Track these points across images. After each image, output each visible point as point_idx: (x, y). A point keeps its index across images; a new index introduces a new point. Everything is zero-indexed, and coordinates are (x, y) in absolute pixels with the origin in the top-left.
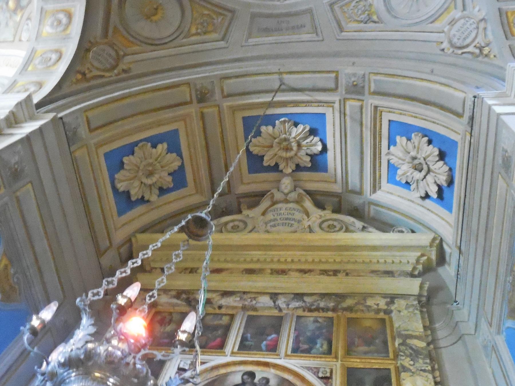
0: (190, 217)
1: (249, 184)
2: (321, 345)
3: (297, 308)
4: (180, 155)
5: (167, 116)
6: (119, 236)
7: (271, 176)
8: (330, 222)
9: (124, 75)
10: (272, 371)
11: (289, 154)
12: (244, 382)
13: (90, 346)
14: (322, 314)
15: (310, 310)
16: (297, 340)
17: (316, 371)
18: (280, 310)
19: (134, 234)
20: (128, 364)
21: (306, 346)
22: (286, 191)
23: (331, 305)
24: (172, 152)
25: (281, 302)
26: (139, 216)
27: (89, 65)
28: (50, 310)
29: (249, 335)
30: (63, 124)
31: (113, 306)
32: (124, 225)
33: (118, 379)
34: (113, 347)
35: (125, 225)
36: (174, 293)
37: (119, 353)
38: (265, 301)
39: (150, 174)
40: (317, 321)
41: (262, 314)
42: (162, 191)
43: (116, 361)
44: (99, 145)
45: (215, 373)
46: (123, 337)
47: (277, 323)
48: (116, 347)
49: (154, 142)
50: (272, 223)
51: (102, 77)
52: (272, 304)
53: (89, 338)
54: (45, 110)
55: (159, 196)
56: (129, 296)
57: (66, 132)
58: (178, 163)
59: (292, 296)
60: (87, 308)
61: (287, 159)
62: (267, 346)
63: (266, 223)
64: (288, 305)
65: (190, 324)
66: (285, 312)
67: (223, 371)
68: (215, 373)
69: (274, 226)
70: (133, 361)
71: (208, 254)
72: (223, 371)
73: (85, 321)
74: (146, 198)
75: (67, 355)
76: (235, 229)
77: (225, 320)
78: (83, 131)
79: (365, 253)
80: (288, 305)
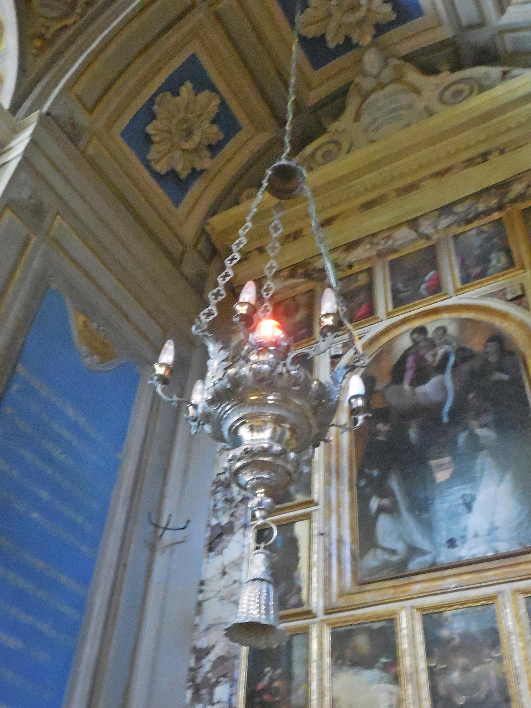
0: (269, 172)
1: (320, 84)
2: (497, 260)
3: (449, 226)
4: (213, 89)
5: (172, 41)
6: (189, 231)
7: (346, 59)
8: (454, 88)
9: (91, 11)
10: (446, 315)
11: (359, 15)
12: (416, 343)
13: (231, 371)
14: (484, 220)
15: (468, 222)
16: (464, 267)
17: (500, 294)
18: (428, 237)
19: (205, 222)
20: (281, 374)
21: (478, 270)
22: (375, 72)
23: (494, 202)
24: (201, 91)
25: (426, 227)
26: (201, 195)
27: (41, 21)
28: (168, 352)
29: (400, 285)
30: (54, 118)
31: (236, 319)
32: (188, 215)
33: (277, 394)
34: (256, 363)
35: (188, 216)
36: (286, 273)
37: (266, 367)
38: (404, 234)
39: (189, 134)
40: (482, 232)
41: (407, 252)
42: (214, 149)
43: (267, 376)
44: (109, 127)
45: (377, 346)
46: (262, 348)
47: (430, 257)
48: (261, 362)
49: (172, 86)
50: (373, 127)
51: (65, 27)
52: (412, 235)
53: (226, 364)
54: (24, 113)
55: (212, 157)
56: (246, 300)
57: (59, 128)
58: (216, 102)
59: (437, 213)
60: (207, 333)
61: (359, 24)
62: (427, 289)
63: (366, 131)
64: (435, 227)
65: (329, 304)
66: (435, 237)
67: (385, 340)
68: (377, 346)
69: (377, 129)
70: (284, 370)
71: (312, 209)
72: (385, 340)
73: (212, 348)
74: (199, 169)
75: (212, 390)
76: (328, 157)
77: (363, 279)
78: (82, 118)
79: (517, 111)
80: (435, 227)
